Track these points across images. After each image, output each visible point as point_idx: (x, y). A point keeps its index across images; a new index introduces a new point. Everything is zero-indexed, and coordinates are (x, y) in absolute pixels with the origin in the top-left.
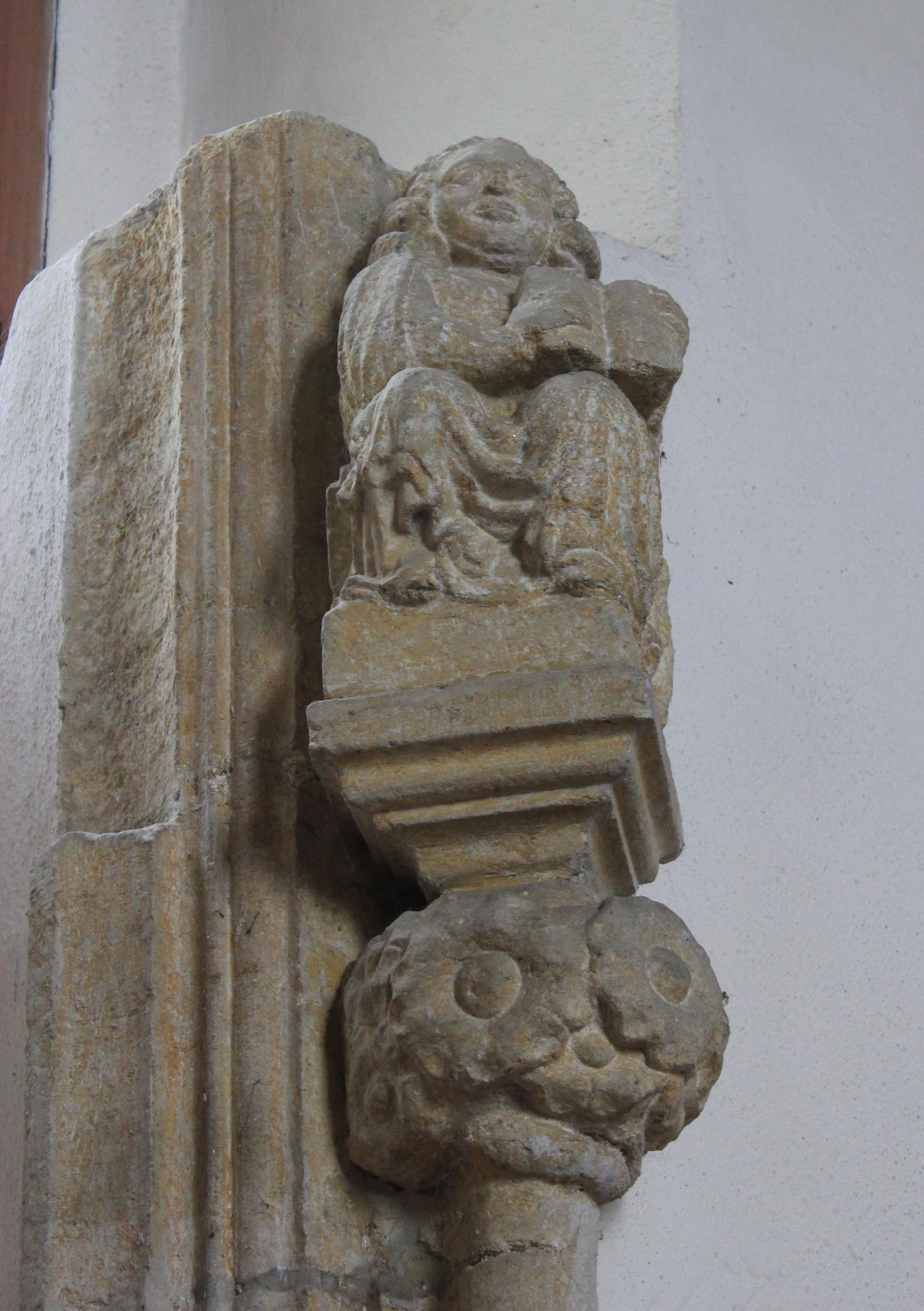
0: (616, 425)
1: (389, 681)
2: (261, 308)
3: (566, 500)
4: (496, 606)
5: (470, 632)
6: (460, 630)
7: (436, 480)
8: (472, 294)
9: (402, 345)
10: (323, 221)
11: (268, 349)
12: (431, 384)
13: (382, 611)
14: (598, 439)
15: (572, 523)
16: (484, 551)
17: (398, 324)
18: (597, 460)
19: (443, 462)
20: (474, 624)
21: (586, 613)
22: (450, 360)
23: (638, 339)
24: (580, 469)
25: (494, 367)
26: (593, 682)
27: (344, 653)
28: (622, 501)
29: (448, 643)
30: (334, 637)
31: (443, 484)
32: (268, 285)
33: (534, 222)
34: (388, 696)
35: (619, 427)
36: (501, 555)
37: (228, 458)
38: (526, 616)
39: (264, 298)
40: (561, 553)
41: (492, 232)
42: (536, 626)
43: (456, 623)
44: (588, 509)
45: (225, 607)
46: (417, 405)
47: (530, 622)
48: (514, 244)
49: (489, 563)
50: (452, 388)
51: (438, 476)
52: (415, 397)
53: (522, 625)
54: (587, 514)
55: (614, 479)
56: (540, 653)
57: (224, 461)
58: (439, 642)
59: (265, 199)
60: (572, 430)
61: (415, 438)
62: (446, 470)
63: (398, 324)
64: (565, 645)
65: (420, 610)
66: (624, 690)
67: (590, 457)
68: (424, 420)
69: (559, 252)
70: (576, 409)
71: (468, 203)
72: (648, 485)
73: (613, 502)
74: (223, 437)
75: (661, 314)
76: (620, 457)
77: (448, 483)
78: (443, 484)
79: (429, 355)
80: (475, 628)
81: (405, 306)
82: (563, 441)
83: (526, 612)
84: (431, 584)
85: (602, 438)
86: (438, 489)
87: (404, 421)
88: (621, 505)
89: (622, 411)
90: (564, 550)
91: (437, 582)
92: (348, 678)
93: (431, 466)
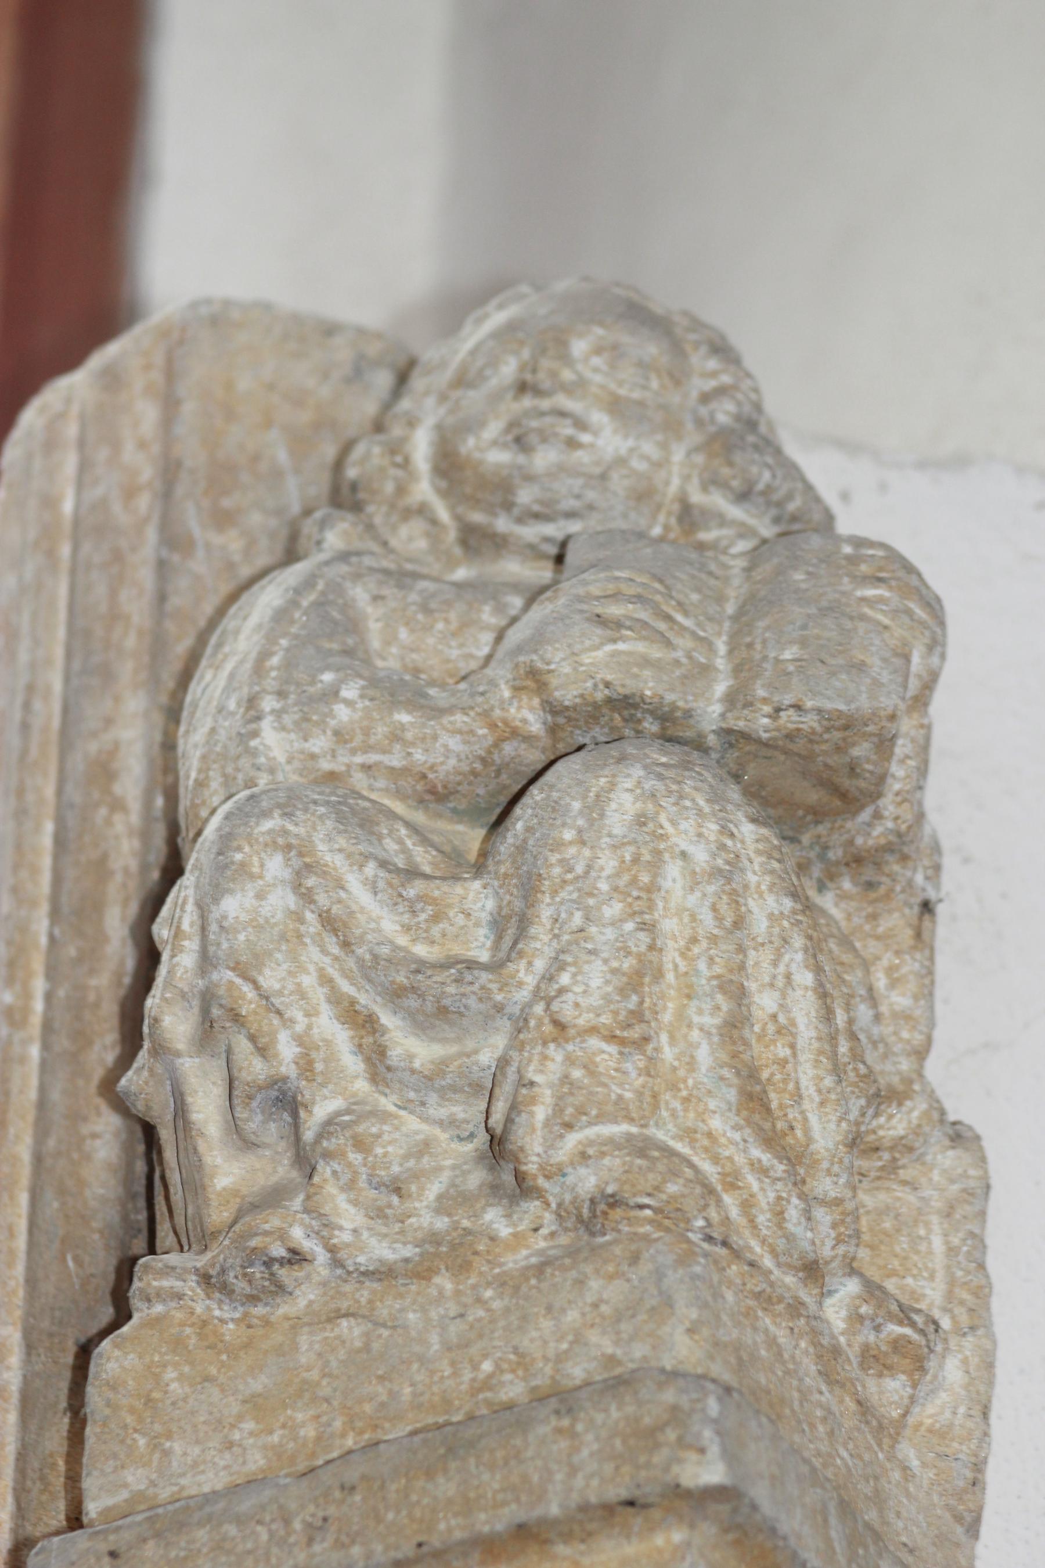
0: (684, 845)
1: (211, 1475)
2: (109, 722)
3: (560, 1025)
4: (429, 1279)
5: (376, 1346)
6: (358, 1344)
7: (292, 1021)
8: (453, 616)
9: (253, 743)
10: (256, 519)
11: (118, 805)
12: (276, 813)
13: (204, 1323)
14: (634, 881)
15: (577, 1074)
16: (411, 1163)
17: (252, 702)
18: (629, 926)
19: (308, 981)
20: (384, 1325)
21: (611, 1268)
22: (359, 759)
23: (787, 655)
24: (590, 952)
25: (452, 762)
26: (599, 1418)
27: (125, 1427)
28: (700, 1012)
29: (330, 1375)
30: (111, 1395)
31: (310, 1027)
32: (127, 670)
33: (630, 443)
34: (187, 1508)
35: (691, 849)
36: (454, 1168)
37: (35, 1051)
38: (489, 1293)
39: (117, 699)
40: (551, 1143)
41: (529, 478)
42: (507, 1310)
43: (350, 1328)
44: (612, 1038)
45: (8, 1368)
46: (243, 865)
47: (496, 1305)
48: (578, 497)
49: (422, 1189)
50: (321, 817)
51: (299, 1016)
52: (239, 849)
53: (481, 1313)
54: (612, 1049)
55: (683, 966)
56: (513, 1371)
57: (23, 1060)
58: (314, 1375)
59: (130, 493)
60: (570, 870)
61: (242, 937)
62: (319, 995)
63: (252, 702)
64: (565, 1346)
65: (281, 1311)
66: (661, 1428)
67: (612, 924)
68: (260, 896)
69: (696, 497)
70: (580, 822)
71: (482, 424)
72: (782, 969)
73: (680, 1015)
74: (26, 1010)
75: (859, 593)
76: (693, 917)
77: (330, 1028)
78: (310, 1027)
79: (313, 757)
80: (385, 1333)
81: (275, 660)
82: (555, 893)
83: (489, 1284)
84: (293, 1251)
85: (645, 878)
86: (299, 1040)
87: (216, 901)
88: (696, 1019)
89: (700, 813)
90: (561, 1136)
91: (309, 1245)
92: (130, 1479)
93: (280, 993)
